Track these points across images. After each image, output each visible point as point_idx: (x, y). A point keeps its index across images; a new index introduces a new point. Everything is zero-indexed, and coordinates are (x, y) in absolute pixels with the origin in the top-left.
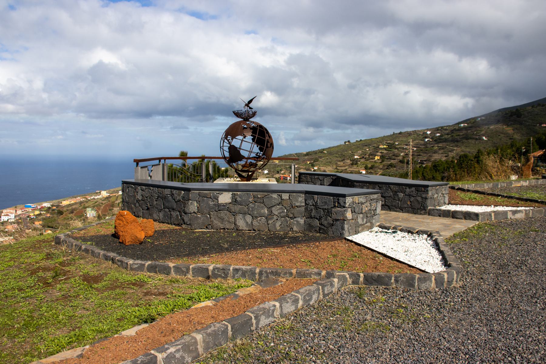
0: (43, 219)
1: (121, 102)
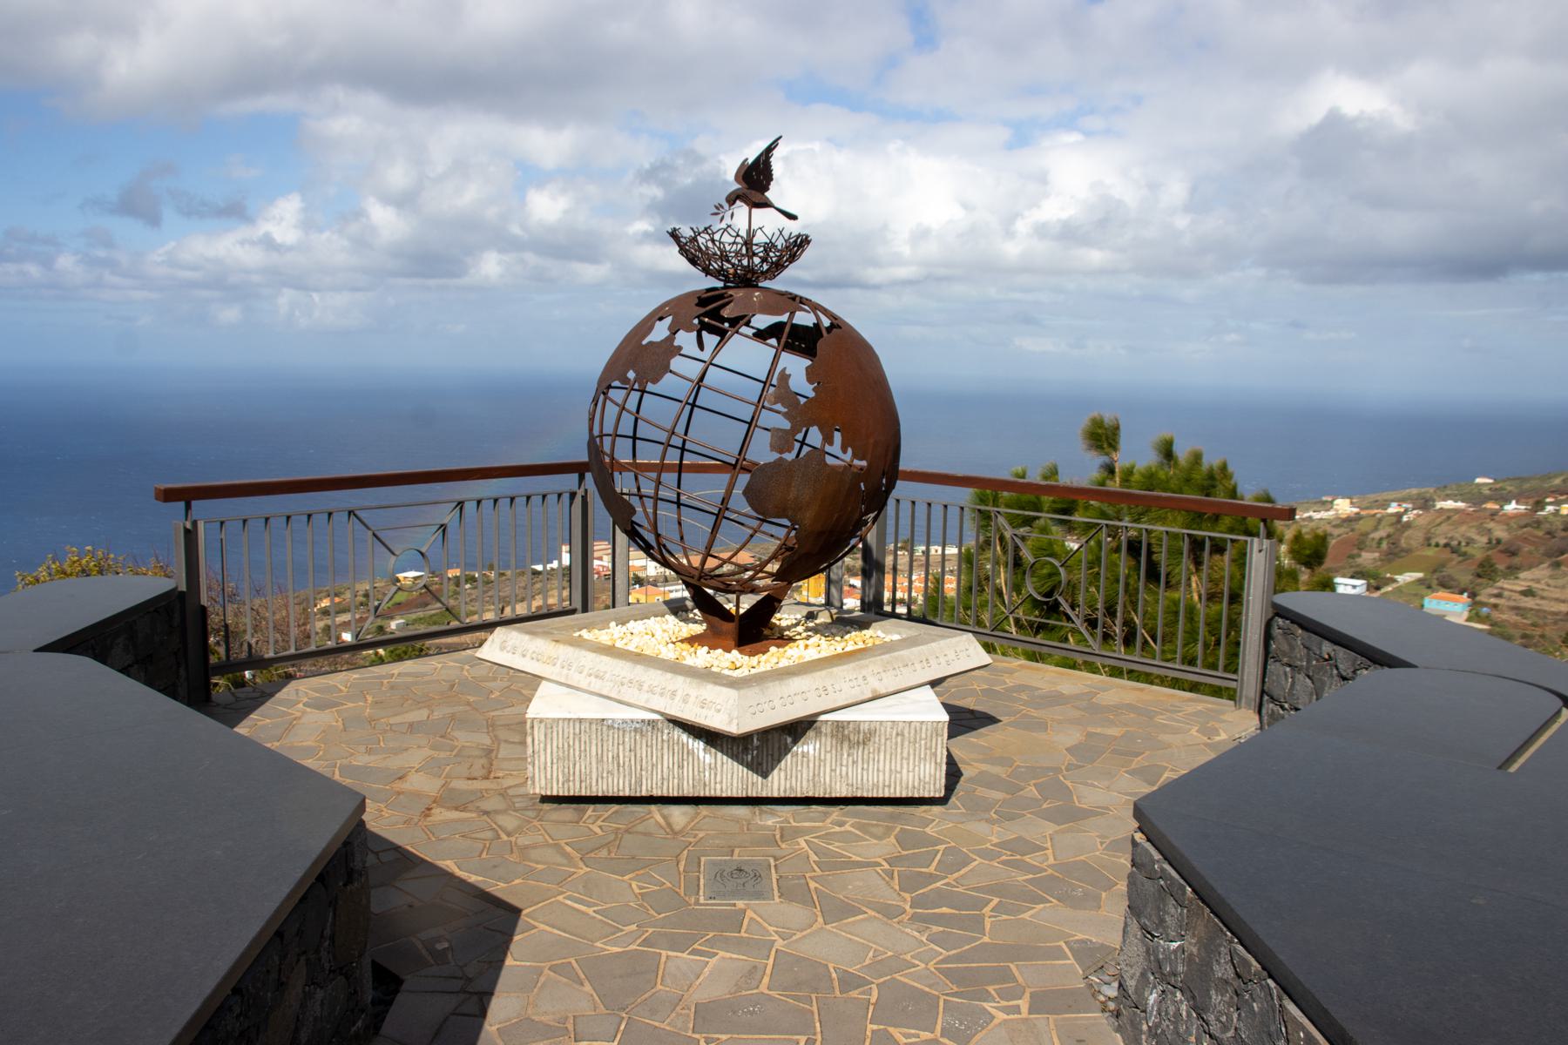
1: (1399, 230)
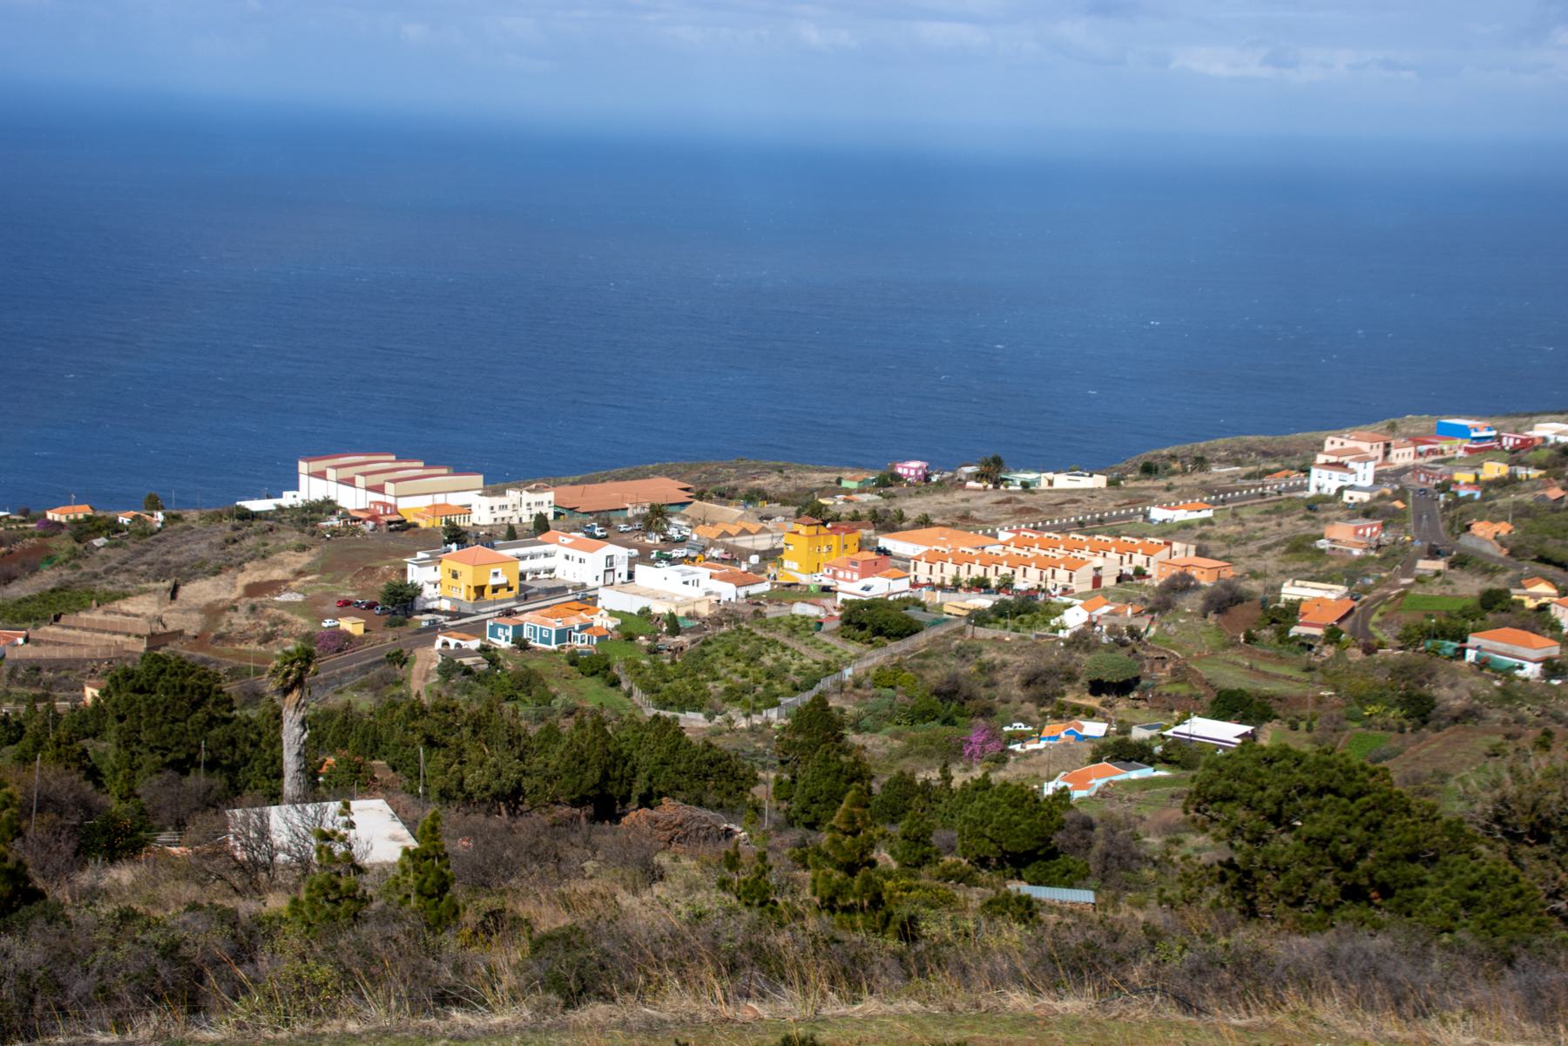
0: (1521, 513)
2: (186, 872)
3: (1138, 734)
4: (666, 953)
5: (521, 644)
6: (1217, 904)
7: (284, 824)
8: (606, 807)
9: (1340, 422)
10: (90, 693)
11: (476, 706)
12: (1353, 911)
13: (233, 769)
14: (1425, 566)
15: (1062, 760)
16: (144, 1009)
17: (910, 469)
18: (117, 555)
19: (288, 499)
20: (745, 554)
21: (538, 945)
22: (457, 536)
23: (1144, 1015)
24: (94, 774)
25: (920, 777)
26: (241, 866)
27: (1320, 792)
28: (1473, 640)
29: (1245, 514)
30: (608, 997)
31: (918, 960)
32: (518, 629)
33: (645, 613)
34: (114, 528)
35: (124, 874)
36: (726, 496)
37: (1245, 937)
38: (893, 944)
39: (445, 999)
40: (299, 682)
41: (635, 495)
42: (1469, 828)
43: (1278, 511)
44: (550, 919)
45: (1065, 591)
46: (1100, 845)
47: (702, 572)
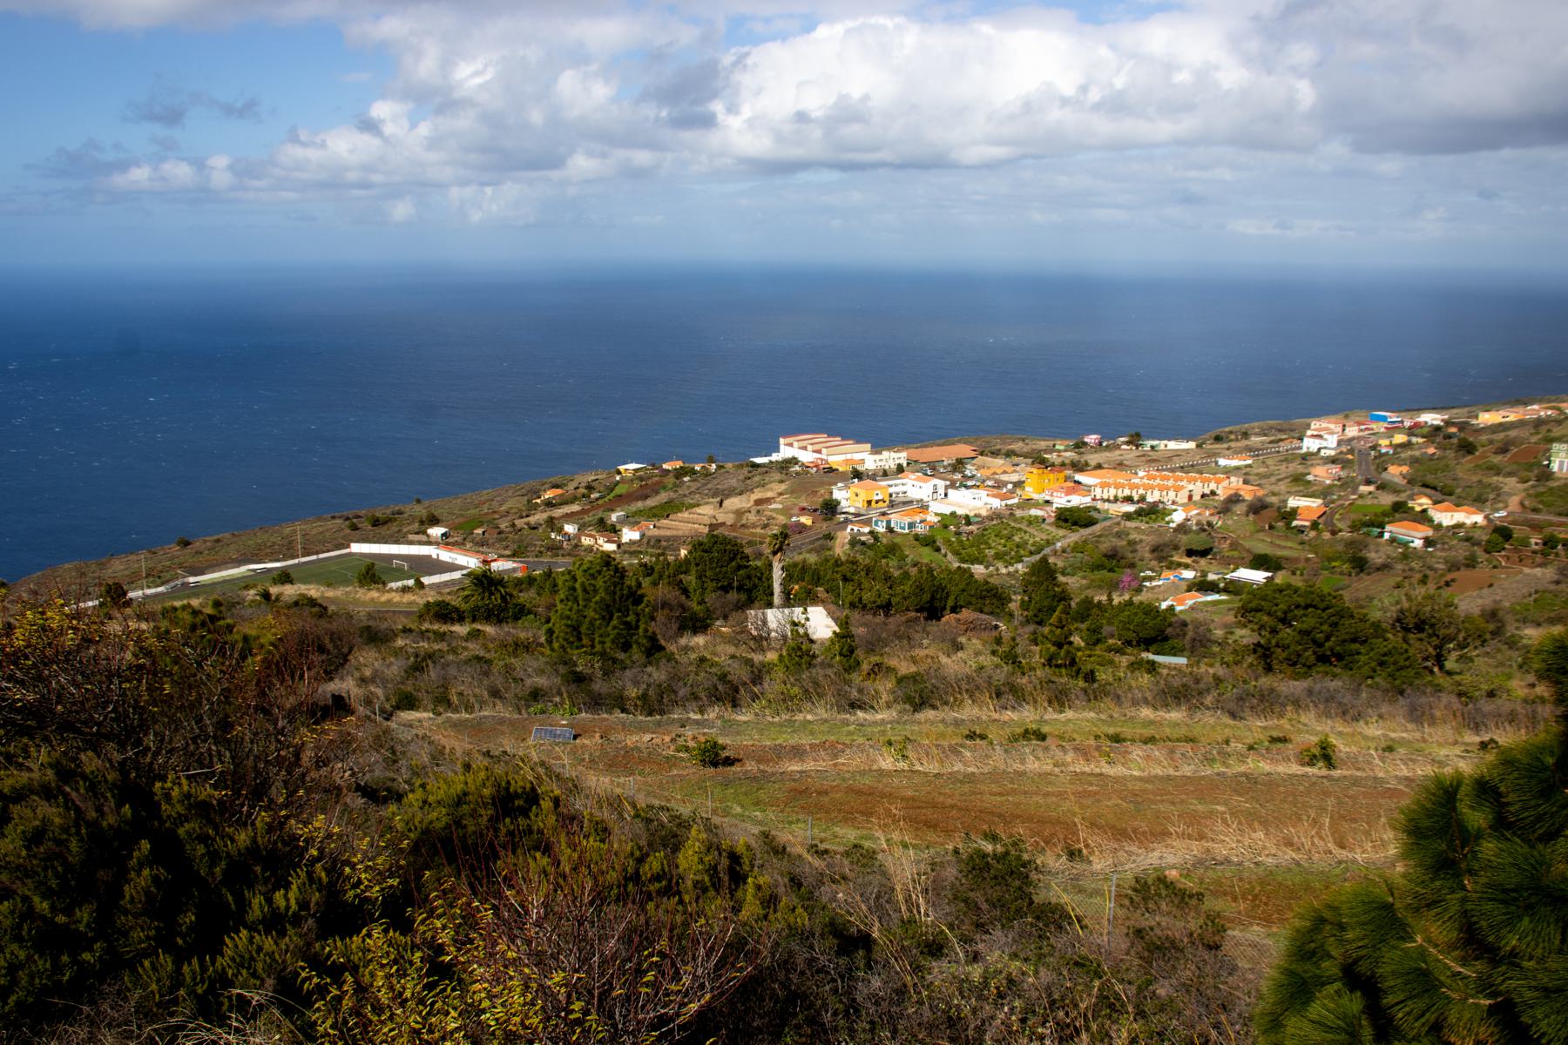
0: (1414, 461)
2: (731, 640)
3: (1211, 577)
4: (964, 686)
5: (890, 530)
6: (1251, 665)
7: (775, 618)
8: (933, 611)
9: (1320, 413)
10: (683, 552)
11: (867, 561)
12: (1322, 668)
13: (749, 591)
14: (1364, 489)
15: (1173, 591)
16: (712, 704)
17: (1091, 439)
18: (694, 486)
19: (775, 457)
20: (1005, 484)
21: (900, 681)
22: (858, 475)
23: (1212, 720)
24: (685, 592)
25: (1096, 599)
26: (754, 638)
27: (1307, 607)
28: (1388, 528)
29: (1269, 462)
30: (934, 707)
31: (1095, 691)
32: (889, 522)
33: (953, 514)
34: (693, 472)
35: (700, 640)
36: (995, 454)
37: (1265, 681)
38: (1081, 683)
39: (854, 706)
40: (780, 549)
41: (947, 454)
42: (1384, 625)
43: (1286, 460)
44: (905, 668)
45: (1174, 503)
46: (1190, 634)
47: (983, 493)
